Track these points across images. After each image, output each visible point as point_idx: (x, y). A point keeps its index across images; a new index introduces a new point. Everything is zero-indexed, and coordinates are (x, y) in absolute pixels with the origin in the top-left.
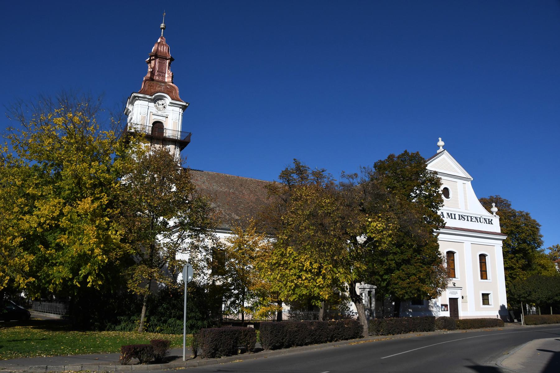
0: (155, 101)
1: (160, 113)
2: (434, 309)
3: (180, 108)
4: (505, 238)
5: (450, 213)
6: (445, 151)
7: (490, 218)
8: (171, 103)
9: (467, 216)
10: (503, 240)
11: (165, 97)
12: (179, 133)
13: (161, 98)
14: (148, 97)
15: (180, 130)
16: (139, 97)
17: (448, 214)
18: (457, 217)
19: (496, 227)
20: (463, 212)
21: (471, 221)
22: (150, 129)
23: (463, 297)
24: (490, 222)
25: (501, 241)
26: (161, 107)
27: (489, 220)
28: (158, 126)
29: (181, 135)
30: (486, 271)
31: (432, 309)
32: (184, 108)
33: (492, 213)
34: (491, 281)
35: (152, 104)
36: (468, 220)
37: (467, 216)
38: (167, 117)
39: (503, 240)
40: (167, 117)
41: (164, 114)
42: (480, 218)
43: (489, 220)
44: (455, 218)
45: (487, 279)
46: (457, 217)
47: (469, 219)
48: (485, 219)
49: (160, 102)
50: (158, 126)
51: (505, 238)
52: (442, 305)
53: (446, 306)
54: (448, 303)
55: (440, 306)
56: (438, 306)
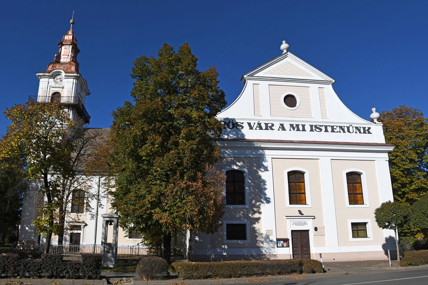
0: (54, 76)
1: (57, 85)
2: (265, 245)
3: (74, 79)
4: (391, 149)
5: (295, 124)
6: (289, 53)
7: (367, 127)
8: (65, 76)
9: (326, 127)
10: (389, 152)
11: (61, 72)
12: (72, 98)
13: (59, 74)
14: (47, 74)
15: (73, 96)
16: (40, 76)
17: (292, 126)
18: (308, 128)
19: (377, 135)
20: (317, 120)
21: (333, 131)
22: (50, 98)
23: (316, 229)
24: (367, 131)
25: (387, 154)
26: (59, 80)
27: (364, 128)
28: (56, 95)
29: (75, 100)
30: (362, 194)
31: (261, 245)
32: (76, 78)
33: (372, 120)
34: (368, 206)
35: (51, 80)
36: (326, 131)
37: (326, 127)
38: (63, 88)
39: (389, 152)
40: (63, 88)
41: (61, 86)
42: (348, 128)
43: (364, 128)
44: (304, 130)
45: (363, 204)
46: (308, 128)
47: (329, 129)
48: (357, 128)
49: (58, 77)
50: (56, 95)
51: (391, 149)
52: (278, 240)
53: (286, 240)
54: (289, 237)
55: (275, 240)
56: (271, 241)
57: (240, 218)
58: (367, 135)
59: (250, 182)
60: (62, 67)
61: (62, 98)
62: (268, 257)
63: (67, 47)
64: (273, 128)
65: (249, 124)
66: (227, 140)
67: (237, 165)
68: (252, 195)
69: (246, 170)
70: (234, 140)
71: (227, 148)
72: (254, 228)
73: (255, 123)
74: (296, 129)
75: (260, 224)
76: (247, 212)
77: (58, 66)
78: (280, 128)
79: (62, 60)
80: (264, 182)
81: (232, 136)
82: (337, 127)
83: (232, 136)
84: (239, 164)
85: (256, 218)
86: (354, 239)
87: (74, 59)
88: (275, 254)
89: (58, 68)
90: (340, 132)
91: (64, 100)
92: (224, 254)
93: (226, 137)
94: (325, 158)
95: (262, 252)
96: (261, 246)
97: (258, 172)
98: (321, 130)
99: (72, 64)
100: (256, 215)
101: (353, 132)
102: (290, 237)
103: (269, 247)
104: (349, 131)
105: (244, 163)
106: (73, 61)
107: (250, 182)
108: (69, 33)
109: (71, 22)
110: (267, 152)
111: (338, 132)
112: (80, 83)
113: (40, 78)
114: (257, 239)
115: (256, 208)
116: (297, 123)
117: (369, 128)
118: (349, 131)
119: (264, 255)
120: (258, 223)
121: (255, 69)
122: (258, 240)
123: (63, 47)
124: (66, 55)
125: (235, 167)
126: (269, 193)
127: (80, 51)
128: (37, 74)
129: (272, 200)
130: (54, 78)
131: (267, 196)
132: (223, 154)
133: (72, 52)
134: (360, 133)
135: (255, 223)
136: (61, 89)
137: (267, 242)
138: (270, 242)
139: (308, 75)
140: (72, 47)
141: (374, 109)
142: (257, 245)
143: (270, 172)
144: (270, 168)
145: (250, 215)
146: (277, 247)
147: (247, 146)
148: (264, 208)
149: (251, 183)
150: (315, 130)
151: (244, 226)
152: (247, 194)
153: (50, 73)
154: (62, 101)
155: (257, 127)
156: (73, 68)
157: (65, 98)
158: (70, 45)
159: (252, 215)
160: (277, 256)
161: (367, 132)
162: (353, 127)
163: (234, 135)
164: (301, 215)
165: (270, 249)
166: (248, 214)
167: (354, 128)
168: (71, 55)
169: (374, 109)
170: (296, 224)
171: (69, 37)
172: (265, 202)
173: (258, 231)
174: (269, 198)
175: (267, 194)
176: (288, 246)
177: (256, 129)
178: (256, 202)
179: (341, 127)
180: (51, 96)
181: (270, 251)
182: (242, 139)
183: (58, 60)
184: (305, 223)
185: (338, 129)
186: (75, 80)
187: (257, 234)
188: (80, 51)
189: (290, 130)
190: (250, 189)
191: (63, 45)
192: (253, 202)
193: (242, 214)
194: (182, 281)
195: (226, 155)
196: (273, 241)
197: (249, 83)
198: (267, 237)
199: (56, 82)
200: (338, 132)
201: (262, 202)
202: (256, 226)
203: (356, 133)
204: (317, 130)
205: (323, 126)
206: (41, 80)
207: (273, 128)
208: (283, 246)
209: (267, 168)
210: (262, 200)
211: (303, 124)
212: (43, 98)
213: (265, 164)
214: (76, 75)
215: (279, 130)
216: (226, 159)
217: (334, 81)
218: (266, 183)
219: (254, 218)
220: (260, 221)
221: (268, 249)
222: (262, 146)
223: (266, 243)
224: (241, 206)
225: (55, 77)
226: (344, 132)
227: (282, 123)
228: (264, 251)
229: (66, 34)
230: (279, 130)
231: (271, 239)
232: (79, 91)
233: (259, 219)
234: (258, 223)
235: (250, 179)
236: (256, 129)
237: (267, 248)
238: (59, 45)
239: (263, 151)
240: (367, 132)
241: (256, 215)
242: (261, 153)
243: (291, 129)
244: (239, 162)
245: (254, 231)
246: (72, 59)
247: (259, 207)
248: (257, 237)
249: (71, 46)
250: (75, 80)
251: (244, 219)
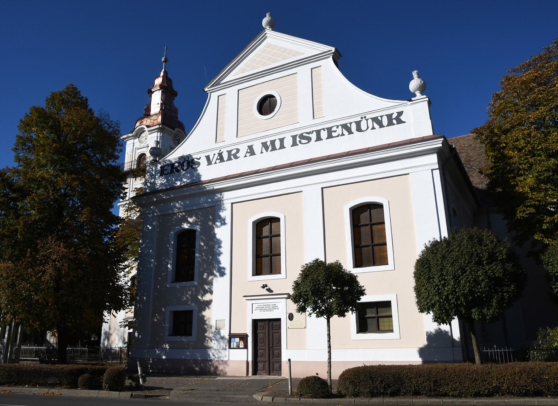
0: (138, 135)
1: (142, 145)
2: (213, 344)
3: (158, 132)
8: (149, 131)
13: (142, 131)
14: (130, 135)
21: (330, 136)
22: (136, 163)
24: (396, 119)
42: (358, 124)
43: (389, 117)
49: (143, 135)
52: (232, 336)
53: (243, 337)
56: (223, 338)
57: (186, 303)
58: (397, 127)
59: (202, 244)
62: (216, 364)
64: (238, 155)
65: (208, 158)
66: (180, 187)
67: (188, 222)
68: (203, 266)
69: (198, 228)
70: (187, 185)
71: (176, 200)
72: (203, 316)
73: (214, 154)
74: (270, 148)
75: (211, 309)
76: (196, 291)
78: (247, 152)
79: (152, 112)
80: (219, 242)
81: (185, 180)
82: (338, 127)
83: (185, 180)
84: (190, 220)
85: (207, 301)
86: (360, 334)
88: (226, 359)
90: (343, 135)
92: (164, 357)
93: (178, 183)
94: (311, 187)
95: (209, 355)
96: (210, 345)
97: (214, 228)
98: (309, 139)
100: (207, 297)
101: (368, 128)
102: (250, 333)
103: (218, 348)
104: (359, 129)
105: (196, 218)
107: (202, 244)
110: (226, 195)
111: (338, 136)
114: (206, 334)
115: (207, 285)
116: (273, 138)
117: (400, 114)
118: (359, 129)
119: (211, 361)
121: (218, 73)
122: (207, 337)
125: (186, 226)
126: (224, 260)
129: (227, 271)
130: (139, 138)
131: (221, 266)
132: (172, 210)
134: (381, 126)
135: (204, 310)
137: (217, 340)
138: (221, 340)
139: (298, 53)
141: (415, 74)
142: (205, 344)
143: (228, 226)
144: (228, 221)
145: (200, 297)
146: (230, 348)
147: (197, 191)
148: (220, 284)
149: (203, 246)
150: (300, 142)
151: (190, 312)
152: (196, 264)
155: (217, 159)
159: (202, 297)
160: (229, 363)
161: (395, 122)
162: (367, 120)
163: (188, 179)
164: (268, 293)
165: (219, 352)
166: (197, 295)
167: (370, 121)
169: (415, 74)
170: (261, 309)
172: (218, 274)
173: (207, 322)
174: (224, 268)
175: (222, 262)
176: (246, 347)
177: (216, 163)
178: (208, 276)
179: (345, 126)
181: (220, 355)
182: (197, 183)
183: (147, 114)
184: (275, 307)
185: (339, 131)
186: (159, 133)
187: (206, 327)
189: (262, 152)
190: (202, 256)
192: (205, 277)
193: (190, 296)
195: (176, 210)
196: (225, 339)
197: (213, 97)
198: (218, 331)
200: (338, 136)
201: (215, 276)
202: (206, 313)
203: (373, 128)
204: (303, 141)
205: (313, 131)
207: (238, 155)
208: (238, 347)
209: (224, 220)
210: (215, 272)
211: (281, 137)
213: (222, 214)
215: (246, 156)
216: (176, 216)
217: (333, 49)
218: (222, 245)
219: (204, 301)
220: (213, 305)
221: (217, 352)
222: (215, 188)
223: (215, 342)
224: (188, 284)
226: (350, 132)
227: (250, 144)
228: (211, 354)
229: (158, 76)
230: (246, 156)
231: (222, 335)
233: (209, 303)
234: (209, 308)
235: (203, 241)
236: (216, 163)
237: (216, 350)
239: (221, 195)
240: (395, 122)
241: (207, 297)
242: (219, 198)
243: (264, 150)
244: (191, 217)
245: (202, 321)
247: (211, 283)
248: (205, 331)
250: (159, 133)
251: (192, 302)
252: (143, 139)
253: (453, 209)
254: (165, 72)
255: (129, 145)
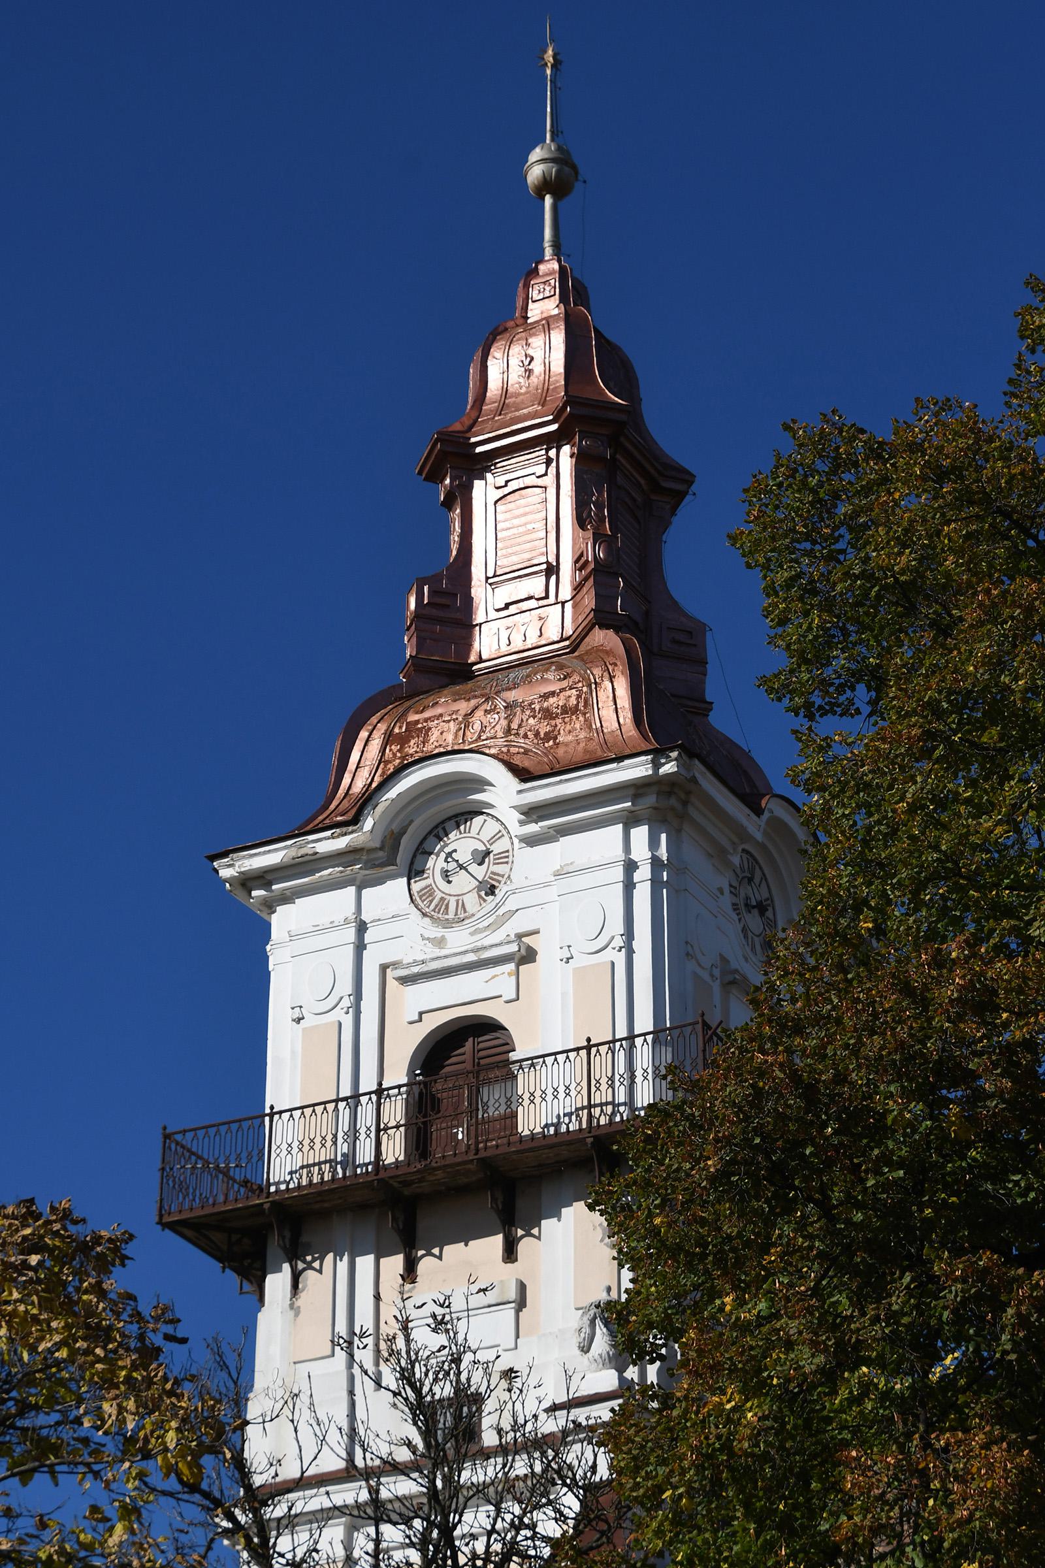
0: (407, 848)
1: (459, 941)
3: (630, 821)
8: (532, 813)
11: (480, 784)
12: (644, 1056)
13: (455, 806)
14: (327, 844)
15: (644, 1022)
16: (264, 877)
22: (395, 1111)
28: (465, 1055)
32: (653, 804)
35: (389, 896)
40: (528, 956)
41: (500, 940)
49: (462, 844)
50: (465, 1055)
60: (490, 722)
61: (524, 1082)
63: (528, 467)
77: (442, 719)
79: (491, 642)
87: (628, 588)
89: (461, 742)
91: (545, 1104)
99: (601, 656)
106: (602, 617)
108: (535, 312)
109: (535, 173)
112: (719, 854)
113: (270, 905)
120: (466, 1245)
123: (482, 492)
124: (519, 574)
127: (687, 478)
128: (227, 871)
130: (414, 872)
133: (581, 520)
136: (501, 980)
140: (580, 459)
143: (623, 1290)
153: (356, 820)
154: (533, 1119)
156: (614, 704)
157: (553, 1075)
158: (552, 441)
168: (579, 562)
171: (528, 363)
180: (397, 1075)
183: (443, 658)
186: (640, 834)
188: (687, 478)
191: (481, 465)
194: (23, 1548)
199: (436, 910)
206: (283, 921)
212: (322, 1123)
214: (637, 769)
225: (423, 851)
229: (505, 323)
232: (727, 939)
234: (466, 1245)
238: (435, 476)
246: (589, 600)
249: (566, 457)
250: (640, 834)
252: (463, 883)
253: (472, 934)
254: (572, 292)
255: (307, 946)
